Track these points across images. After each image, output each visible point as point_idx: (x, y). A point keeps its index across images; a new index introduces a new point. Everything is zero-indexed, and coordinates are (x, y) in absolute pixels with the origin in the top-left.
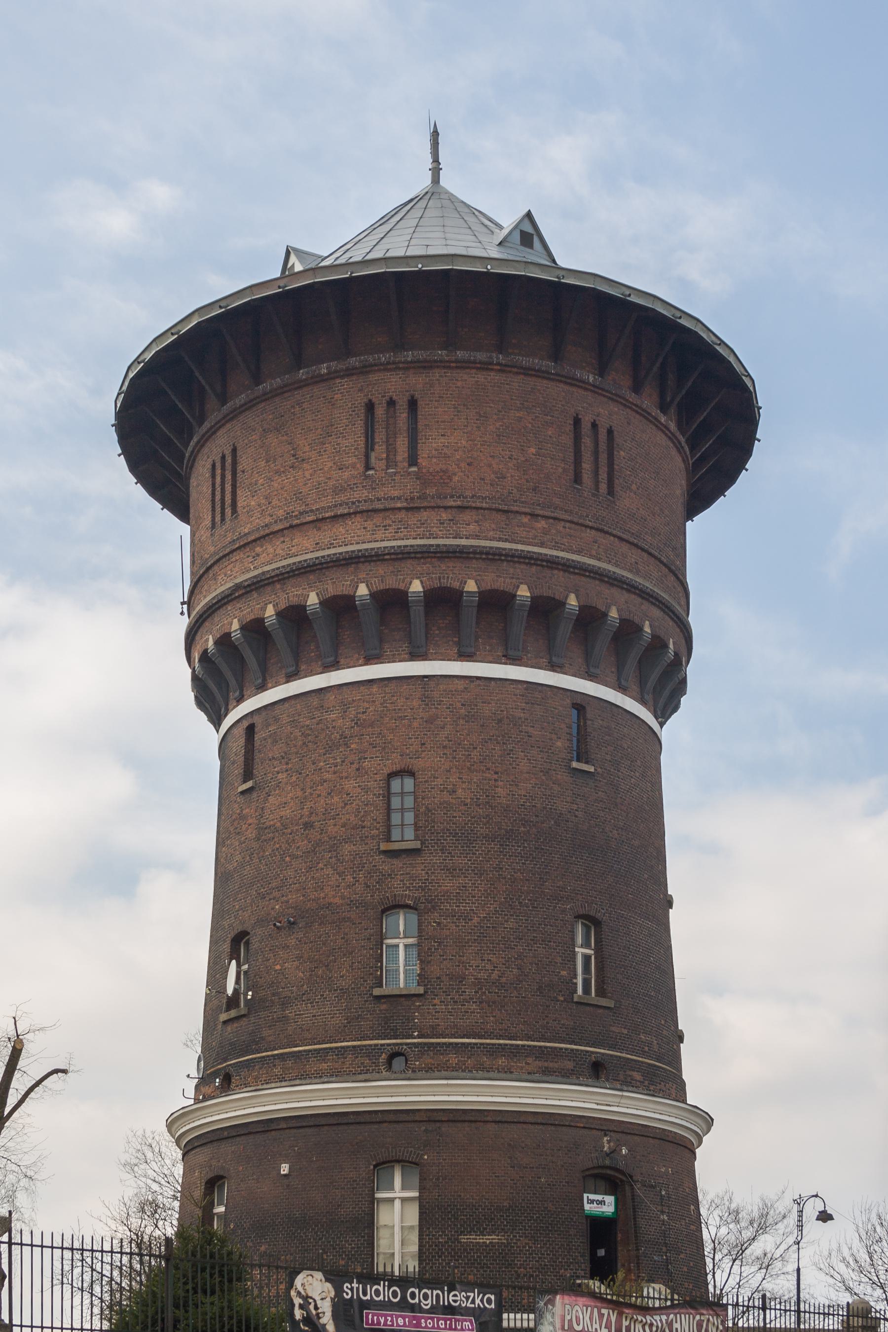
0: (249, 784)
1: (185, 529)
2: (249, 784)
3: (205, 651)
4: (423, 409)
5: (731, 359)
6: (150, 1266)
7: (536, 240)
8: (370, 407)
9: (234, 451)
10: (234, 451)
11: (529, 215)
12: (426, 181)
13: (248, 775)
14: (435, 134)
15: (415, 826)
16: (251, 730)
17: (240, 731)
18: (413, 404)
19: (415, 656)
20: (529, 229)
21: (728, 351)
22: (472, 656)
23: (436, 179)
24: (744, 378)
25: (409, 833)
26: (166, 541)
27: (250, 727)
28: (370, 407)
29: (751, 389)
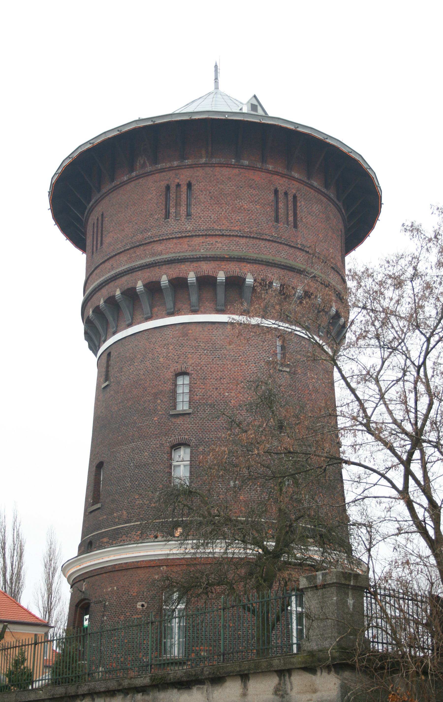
0: (107, 383)
1: (85, 256)
2: (107, 383)
3: (88, 317)
4: (195, 187)
5: (360, 159)
6: (205, 527)
7: (259, 108)
8: (168, 188)
9: (102, 215)
10: (102, 215)
11: (255, 96)
12: (212, 88)
13: (107, 379)
14: (216, 66)
15: (189, 403)
16: (109, 354)
17: (106, 354)
18: (189, 185)
19: (195, 312)
20: (255, 103)
21: (373, 173)
22: (196, 311)
23: (217, 88)
24: (368, 170)
25: (186, 407)
26: (74, 262)
27: (108, 353)
28: (168, 188)
29: (374, 177)
